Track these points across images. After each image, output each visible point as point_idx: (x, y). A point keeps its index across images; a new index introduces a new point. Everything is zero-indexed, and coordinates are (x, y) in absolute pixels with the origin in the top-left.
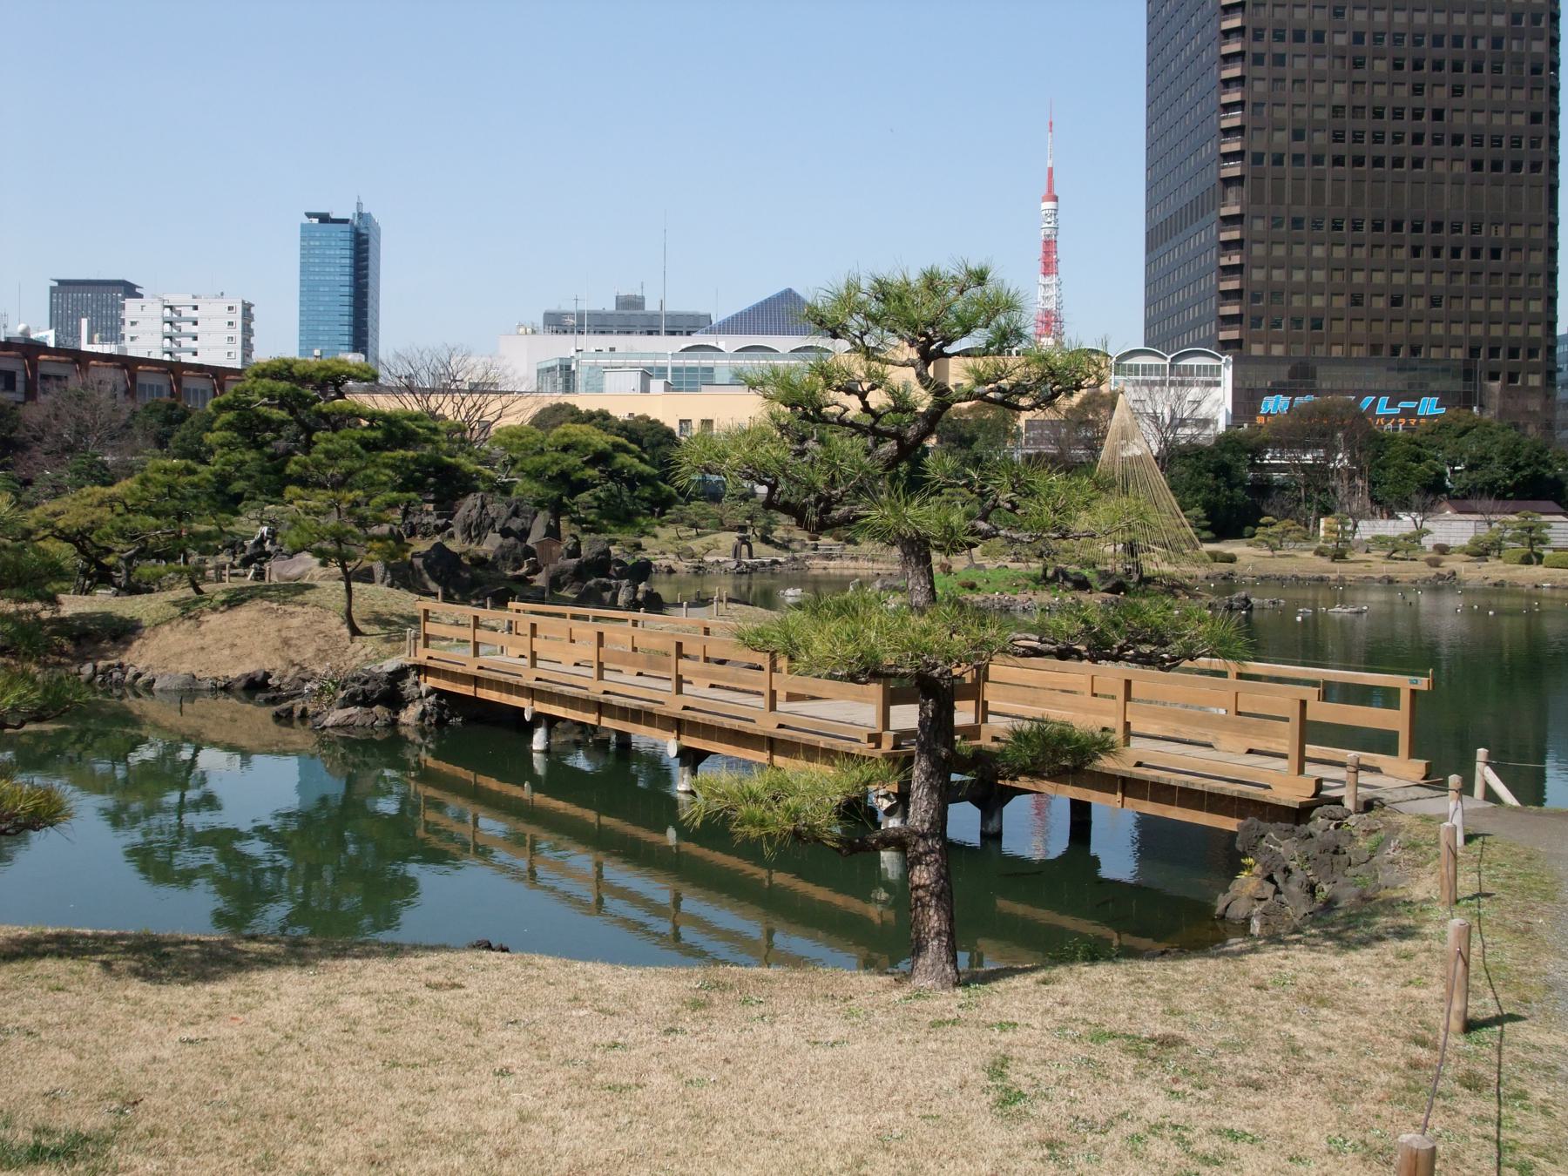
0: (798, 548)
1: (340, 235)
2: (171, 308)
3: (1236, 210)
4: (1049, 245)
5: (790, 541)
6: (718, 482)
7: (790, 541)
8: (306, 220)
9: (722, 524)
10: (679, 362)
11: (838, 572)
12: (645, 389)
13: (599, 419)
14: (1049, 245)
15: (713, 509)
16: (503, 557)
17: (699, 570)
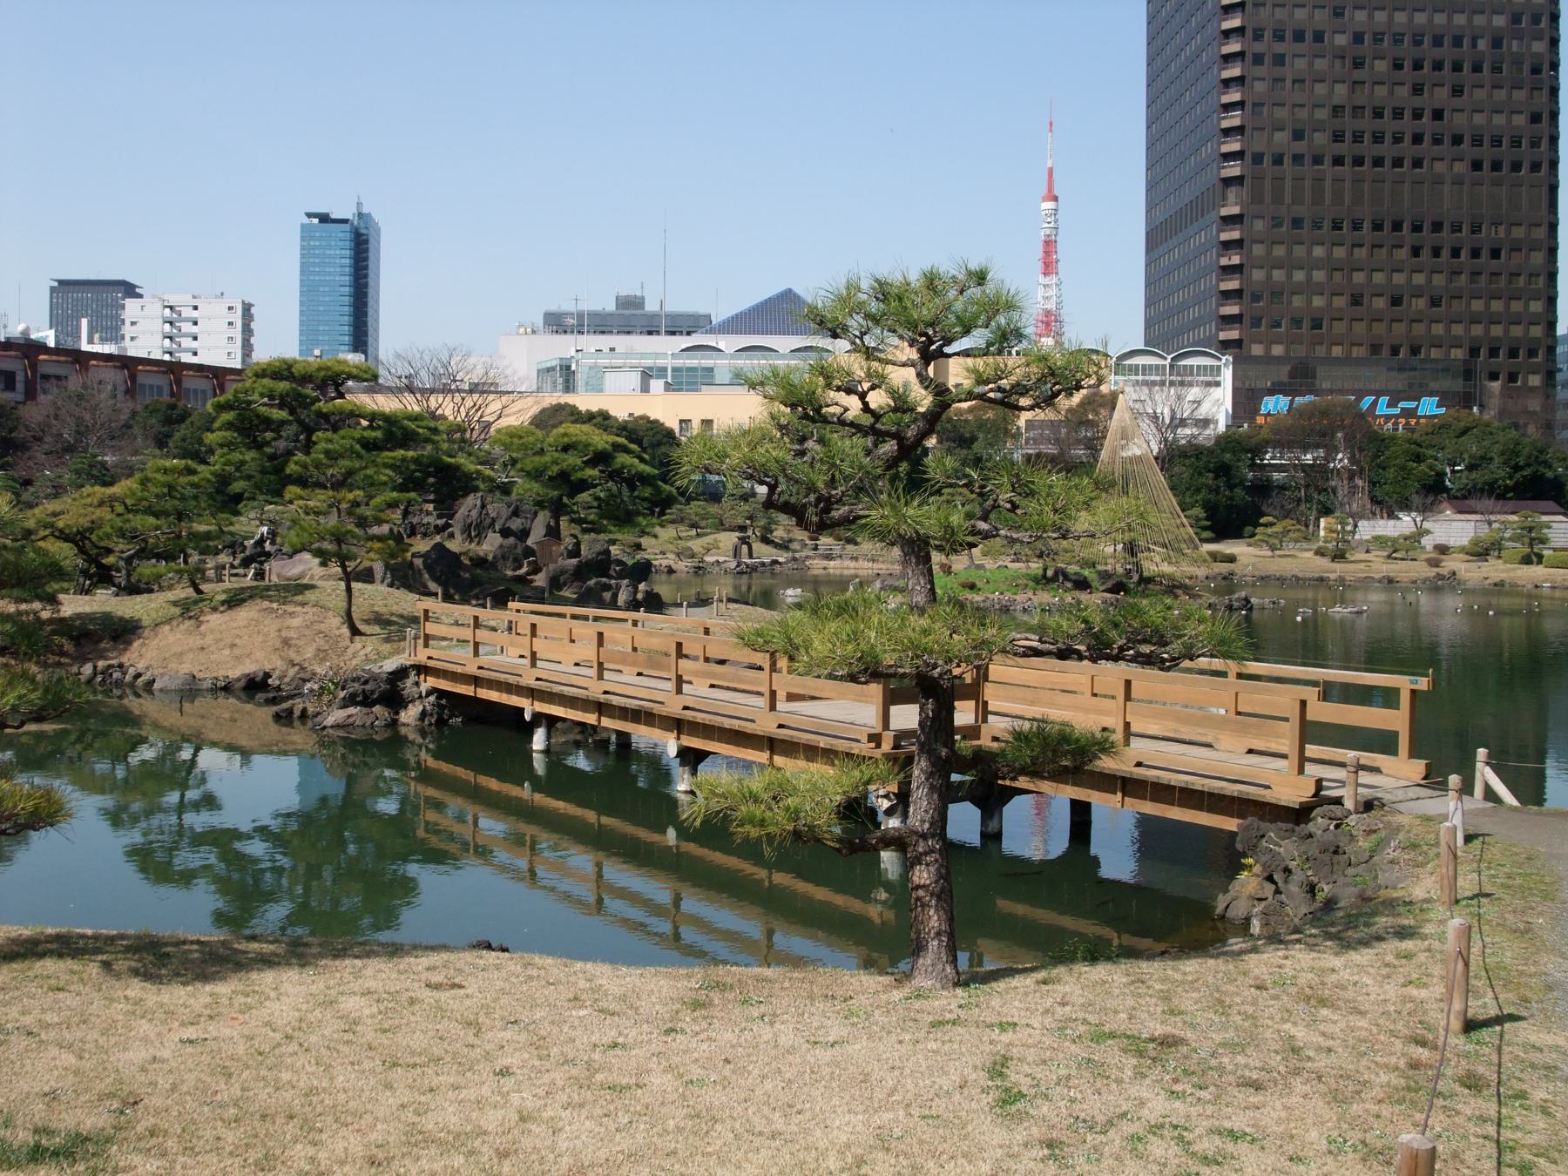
0: (798, 548)
1: (340, 235)
2: (171, 308)
3: (1236, 210)
4: (1049, 245)
5: (790, 541)
6: (718, 482)
7: (790, 541)
8: (306, 220)
9: (722, 524)
10: (679, 362)
11: (838, 572)
12: (645, 389)
13: (599, 419)
14: (1049, 245)
15: (713, 509)
16: (503, 557)
17: (699, 570)
